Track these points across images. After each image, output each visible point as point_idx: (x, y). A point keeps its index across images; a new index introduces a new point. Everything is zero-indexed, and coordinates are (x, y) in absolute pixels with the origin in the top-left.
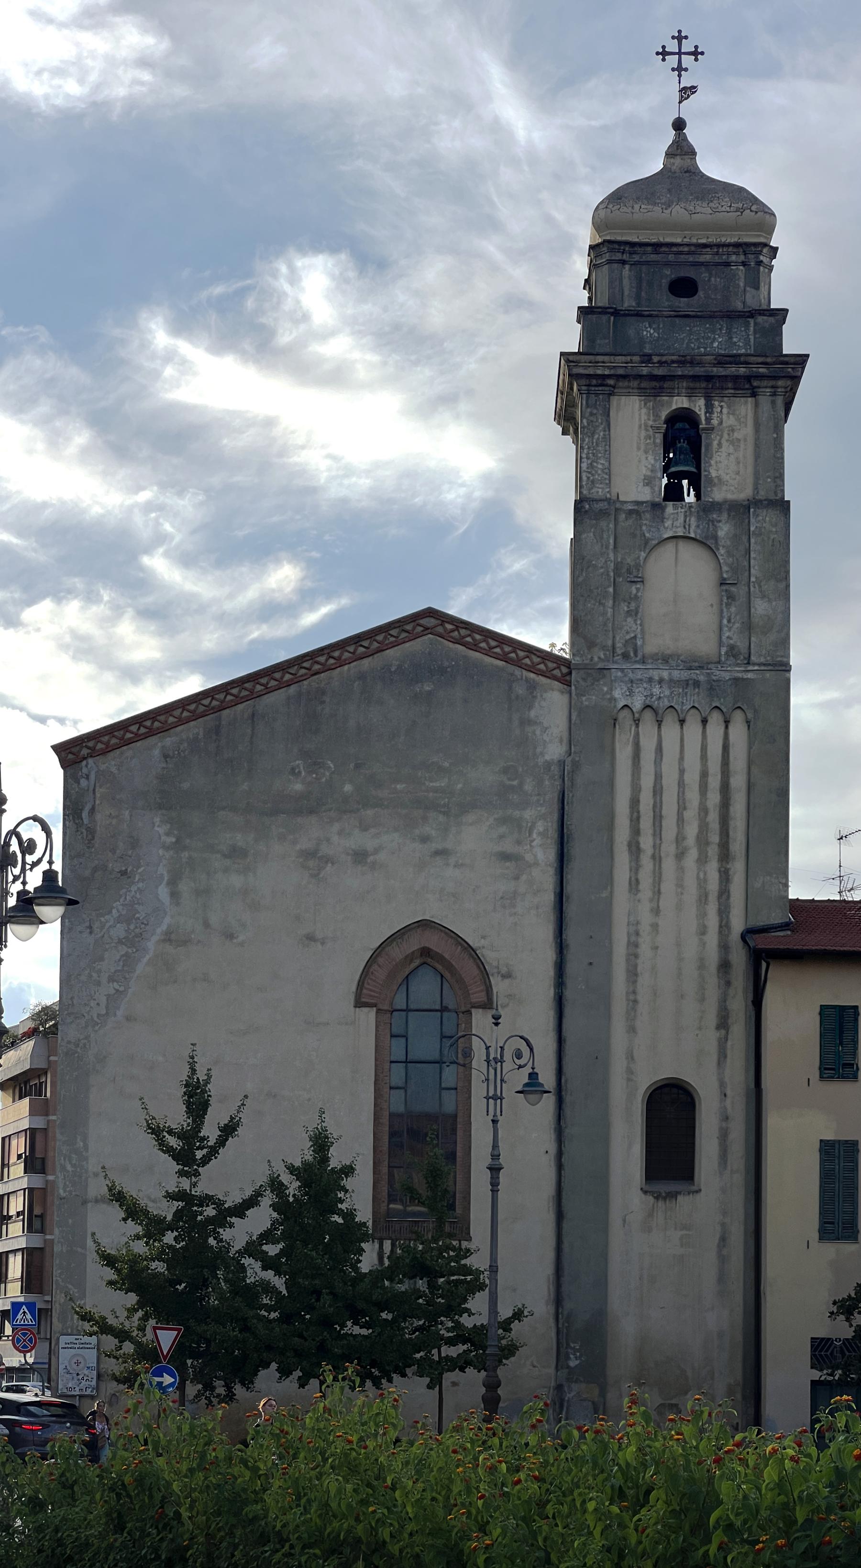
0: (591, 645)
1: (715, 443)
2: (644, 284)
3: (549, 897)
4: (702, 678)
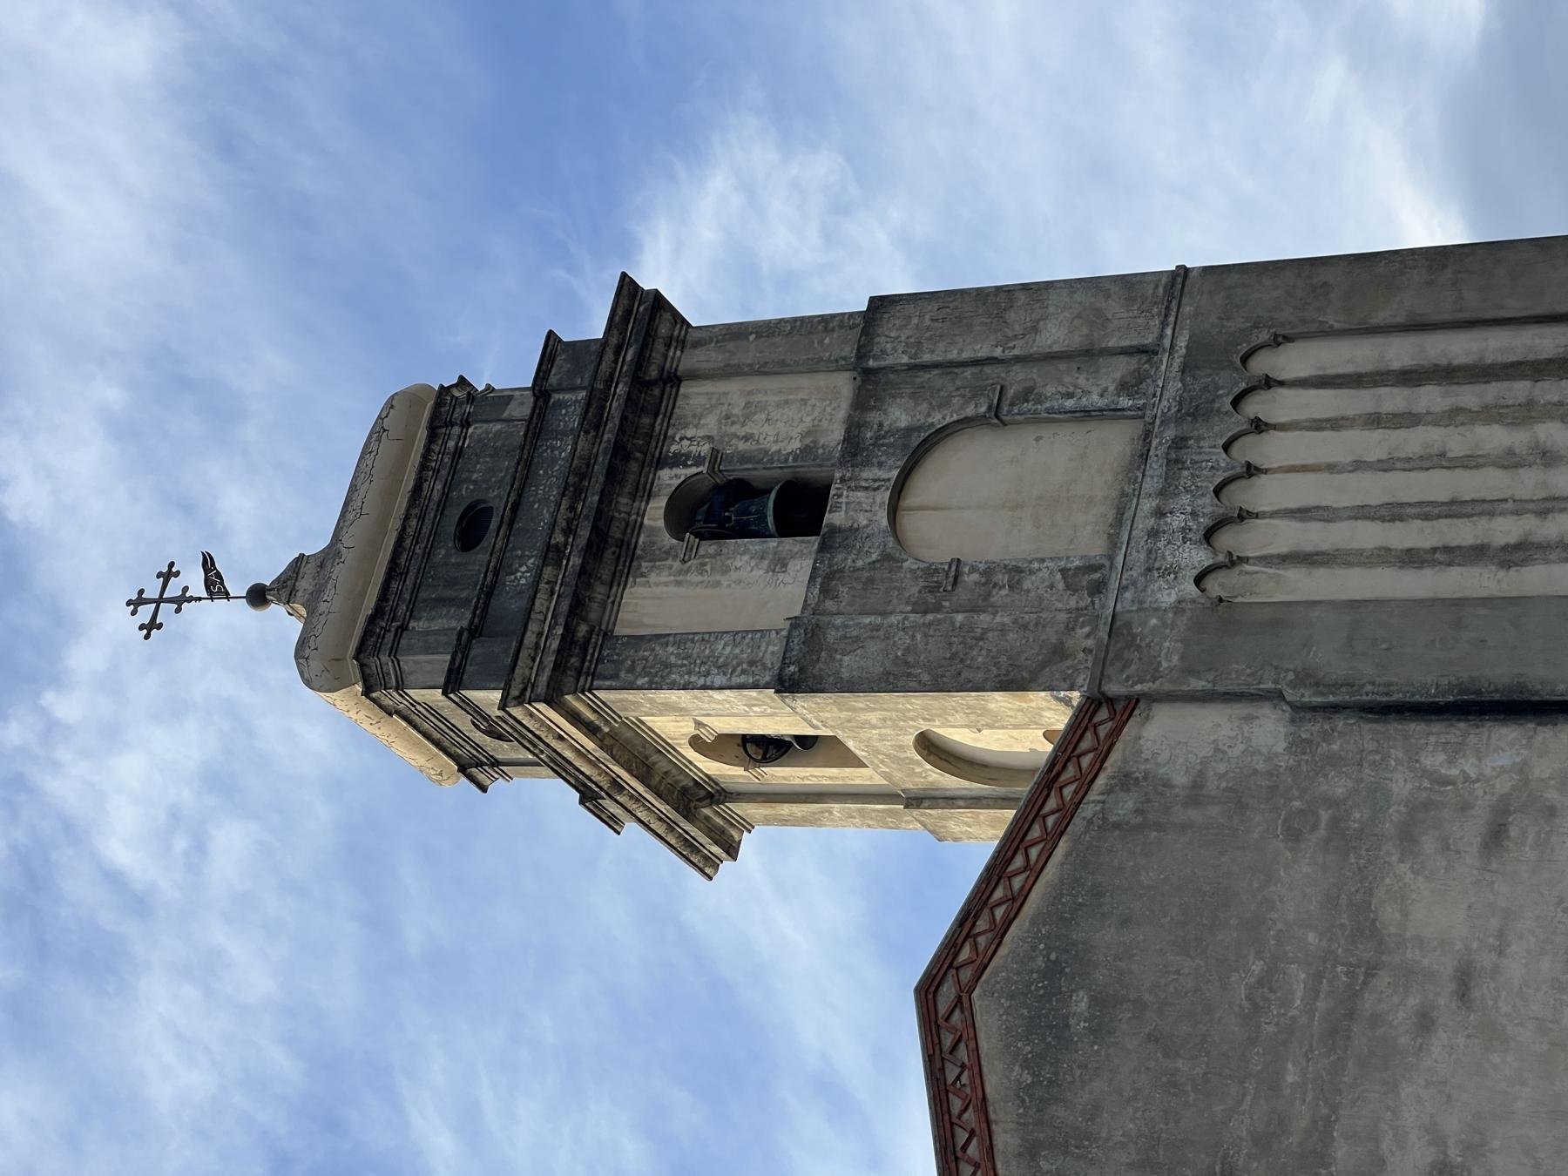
0: (1059, 652)
1: (742, 446)
2: (449, 593)
4: (1170, 434)
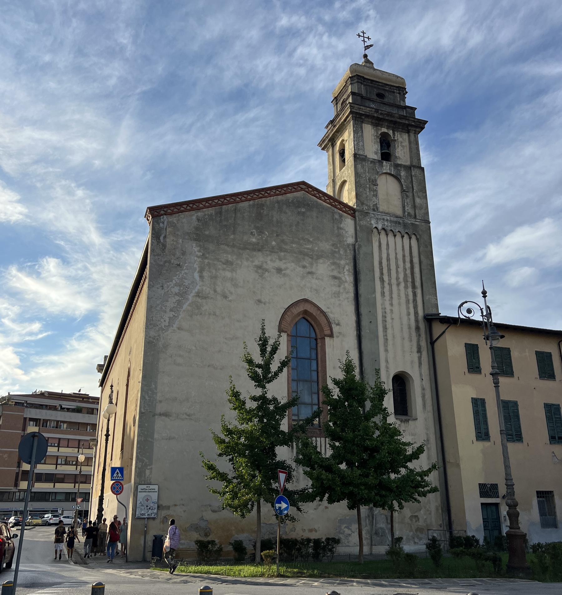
0: (363, 204)
3: (352, 295)
4: (401, 221)
